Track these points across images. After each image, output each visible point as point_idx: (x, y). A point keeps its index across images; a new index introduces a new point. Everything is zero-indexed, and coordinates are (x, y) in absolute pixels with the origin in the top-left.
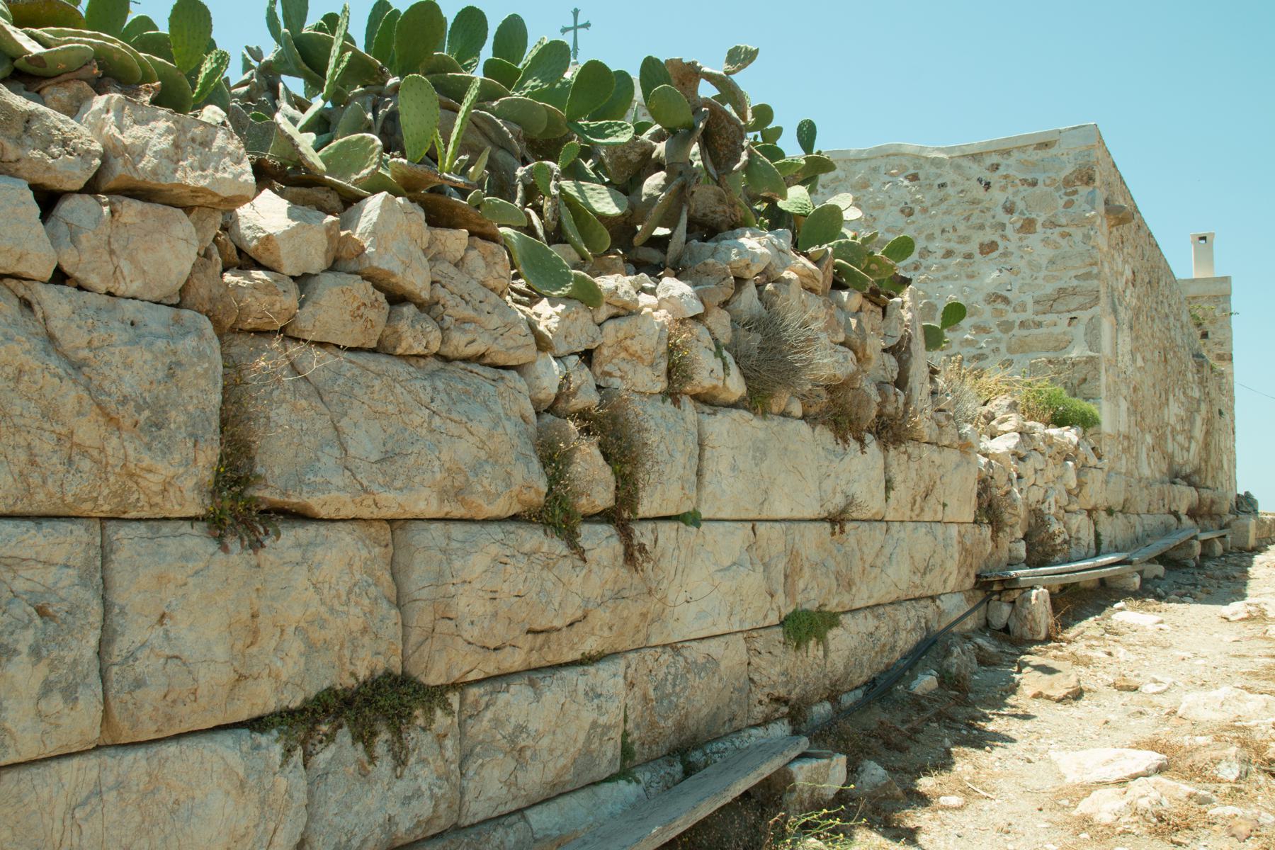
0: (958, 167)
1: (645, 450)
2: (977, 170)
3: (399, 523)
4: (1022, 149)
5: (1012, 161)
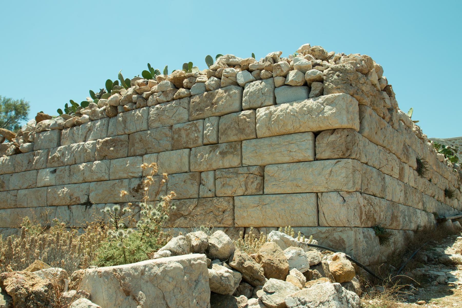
0: (446, 142)
1: (130, 288)
2: (450, 143)
3: (340, 130)
4: (459, 139)
5: (457, 141)
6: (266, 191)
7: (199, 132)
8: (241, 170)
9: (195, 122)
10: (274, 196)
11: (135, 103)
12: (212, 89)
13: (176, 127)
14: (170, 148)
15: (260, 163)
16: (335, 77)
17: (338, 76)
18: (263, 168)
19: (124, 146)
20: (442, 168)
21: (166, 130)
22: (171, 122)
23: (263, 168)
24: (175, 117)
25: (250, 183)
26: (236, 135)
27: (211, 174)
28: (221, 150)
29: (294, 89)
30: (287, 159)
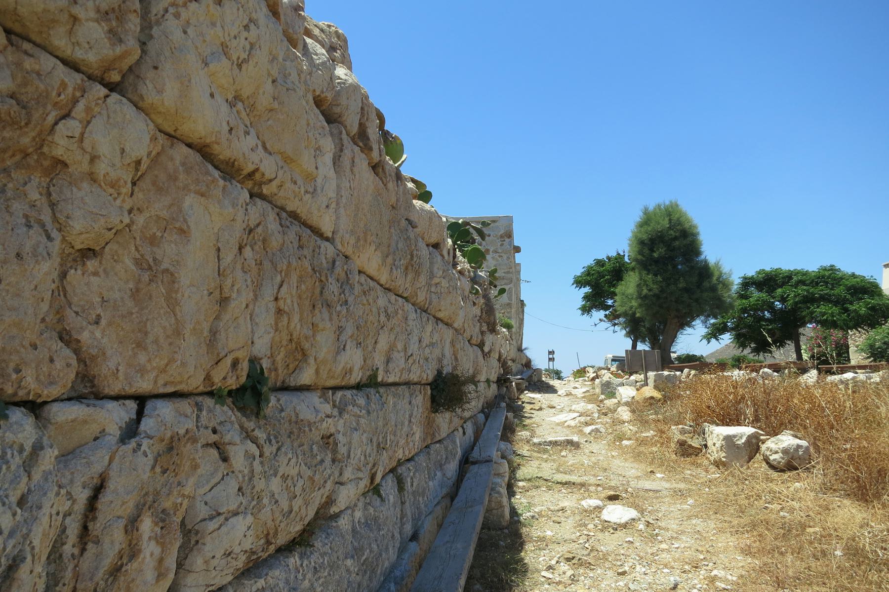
20: (432, 276)
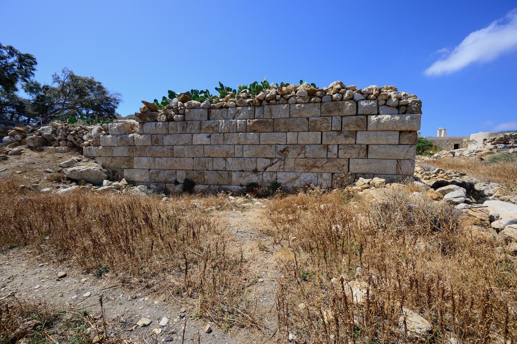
6: (369, 157)
7: (329, 123)
8: (356, 146)
9: (327, 117)
10: (375, 160)
11: (278, 100)
12: (338, 100)
13: (311, 119)
14: (307, 130)
15: (367, 144)
16: (416, 105)
17: (417, 105)
18: (367, 146)
19: (271, 125)
21: (305, 120)
22: (308, 115)
23: (367, 146)
24: (312, 113)
25: (361, 153)
26: (355, 128)
27: (336, 147)
28: (345, 134)
29: (391, 108)
30: (385, 143)
